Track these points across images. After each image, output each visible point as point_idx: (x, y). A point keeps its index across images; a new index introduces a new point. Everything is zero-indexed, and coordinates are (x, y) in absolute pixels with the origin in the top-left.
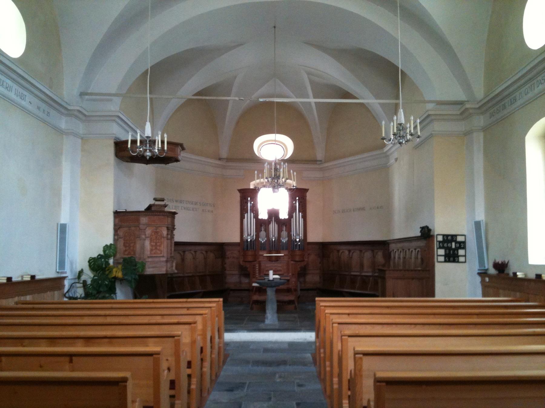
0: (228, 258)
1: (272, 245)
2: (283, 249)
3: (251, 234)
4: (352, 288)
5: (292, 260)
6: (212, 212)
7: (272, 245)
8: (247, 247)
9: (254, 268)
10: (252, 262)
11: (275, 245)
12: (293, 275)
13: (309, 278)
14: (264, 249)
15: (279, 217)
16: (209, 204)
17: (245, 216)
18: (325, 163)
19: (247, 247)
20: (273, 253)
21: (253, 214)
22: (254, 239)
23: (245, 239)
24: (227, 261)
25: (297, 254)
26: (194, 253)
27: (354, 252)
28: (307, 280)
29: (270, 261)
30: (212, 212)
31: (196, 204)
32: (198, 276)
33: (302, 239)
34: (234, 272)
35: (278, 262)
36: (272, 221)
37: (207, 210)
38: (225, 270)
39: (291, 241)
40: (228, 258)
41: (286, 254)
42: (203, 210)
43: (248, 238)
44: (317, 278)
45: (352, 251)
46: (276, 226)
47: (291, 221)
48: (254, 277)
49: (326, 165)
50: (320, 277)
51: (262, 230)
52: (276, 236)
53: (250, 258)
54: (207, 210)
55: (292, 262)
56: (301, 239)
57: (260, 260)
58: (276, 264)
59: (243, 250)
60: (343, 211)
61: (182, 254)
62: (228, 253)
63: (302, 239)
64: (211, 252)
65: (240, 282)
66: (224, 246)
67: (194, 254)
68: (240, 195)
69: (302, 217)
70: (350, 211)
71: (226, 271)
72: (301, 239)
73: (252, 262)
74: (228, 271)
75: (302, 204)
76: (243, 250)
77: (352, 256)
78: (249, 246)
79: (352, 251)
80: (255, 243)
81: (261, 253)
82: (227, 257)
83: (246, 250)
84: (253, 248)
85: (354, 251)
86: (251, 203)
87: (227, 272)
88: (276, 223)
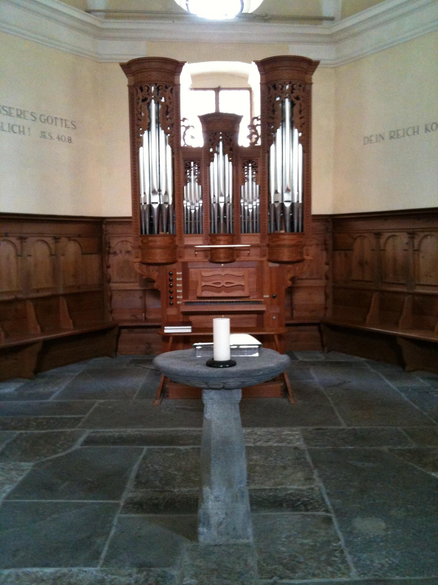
0: (115, 253)
1: (219, 219)
2: (247, 231)
3: (160, 190)
4: (416, 327)
5: (269, 261)
6: (70, 140)
7: (219, 219)
8: (151, 225)
9: (171, 281)
10: (167, 264)
11: (225, 219)
12: (274, 297)
13: (300, 297)
14: (198, 232)
15: (236, 139)
16: (59, 122)
17: (142, 138)
18: (342, 19)
19: (151, 225)
20: (220, 240)
21: (166, 133)
22: (170, 203)
23: (145, 203)
24: (114, 260)
25: (286, 242)
26: (17, 242)
27: (426, 236)
28: (296, 302)
29: (212, 261)
30: (70, 140)
31: (21, 114)
32: (32, 299)
33: (298, 202)
34: (129, 286)
35: (234, 264)
36: (218, 153)
37: (55, 136)
38: (109, 281)
39: (269, 207)
40: (115, 253)
41: (254, 243)
42: (43, 133)
43: (152, 201)
44: (319, 299)
45: (387, 235)
46: (229, 166)
47: (269, 152)
48: (172, 305)
49: (348, 23)
50: (327, 297)
51: (190, 180)
52: (227, 195)
53: (159, 256)
54: (55, 136)
55: (271, 265)
56: (296, 201)
57: (186, 259)
58: (228, 271)
59: (142, 233)
60: (394, 135)
61: (422, 234)
62: (115, 243)
63: (298, 202)
64: (69, 239)
65: (145, 309)
66: (104, 226)
67: (19, 248)
68: (129, 82)
69: (300, 140)
70: (416, 131)
71: (111, 285)
72: (296, 201)
73: (167, 264)
74: (116, 283)
75: (301, 105)
76: (142, 233)
77: (419, 245)
78: (156, 222)
79: (387, 235)
80: (171, 212)
81: (189, 241)
82: (112, 251)
83: (148, 233)
84: (167, 230)
85: (390, 234)
86: (158, 103)
87: (113, 286)
88: (229, 157)
